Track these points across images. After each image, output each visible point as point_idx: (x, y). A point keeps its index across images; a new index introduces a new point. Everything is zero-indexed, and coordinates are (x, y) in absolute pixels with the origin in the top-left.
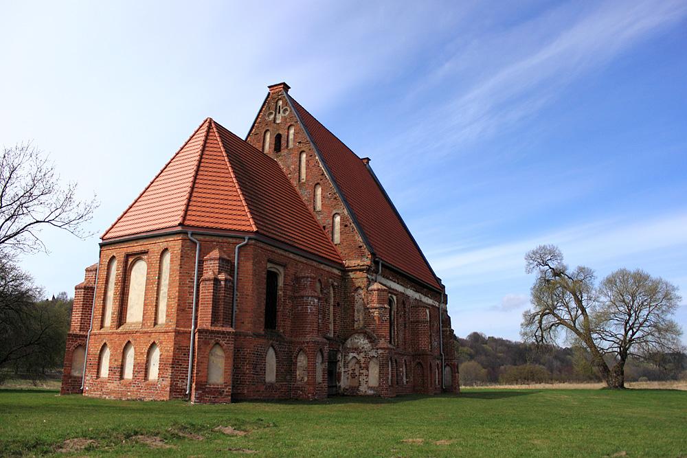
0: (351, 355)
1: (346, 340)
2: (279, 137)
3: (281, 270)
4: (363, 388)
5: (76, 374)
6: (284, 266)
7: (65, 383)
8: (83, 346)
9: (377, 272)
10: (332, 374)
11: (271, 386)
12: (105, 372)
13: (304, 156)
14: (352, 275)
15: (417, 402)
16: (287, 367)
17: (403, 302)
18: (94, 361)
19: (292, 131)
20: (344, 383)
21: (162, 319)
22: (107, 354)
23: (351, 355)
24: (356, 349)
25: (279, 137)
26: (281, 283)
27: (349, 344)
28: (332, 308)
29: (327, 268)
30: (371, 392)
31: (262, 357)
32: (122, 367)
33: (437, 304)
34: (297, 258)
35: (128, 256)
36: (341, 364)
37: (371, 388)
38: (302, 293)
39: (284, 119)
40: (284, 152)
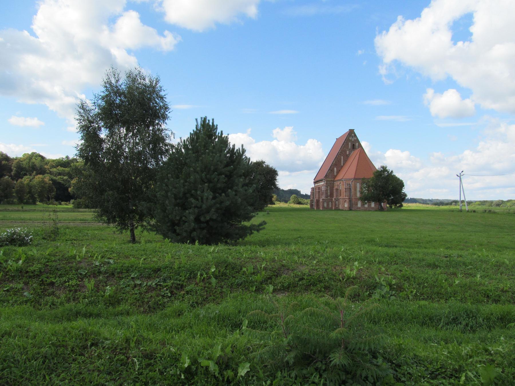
25: (354, 145)
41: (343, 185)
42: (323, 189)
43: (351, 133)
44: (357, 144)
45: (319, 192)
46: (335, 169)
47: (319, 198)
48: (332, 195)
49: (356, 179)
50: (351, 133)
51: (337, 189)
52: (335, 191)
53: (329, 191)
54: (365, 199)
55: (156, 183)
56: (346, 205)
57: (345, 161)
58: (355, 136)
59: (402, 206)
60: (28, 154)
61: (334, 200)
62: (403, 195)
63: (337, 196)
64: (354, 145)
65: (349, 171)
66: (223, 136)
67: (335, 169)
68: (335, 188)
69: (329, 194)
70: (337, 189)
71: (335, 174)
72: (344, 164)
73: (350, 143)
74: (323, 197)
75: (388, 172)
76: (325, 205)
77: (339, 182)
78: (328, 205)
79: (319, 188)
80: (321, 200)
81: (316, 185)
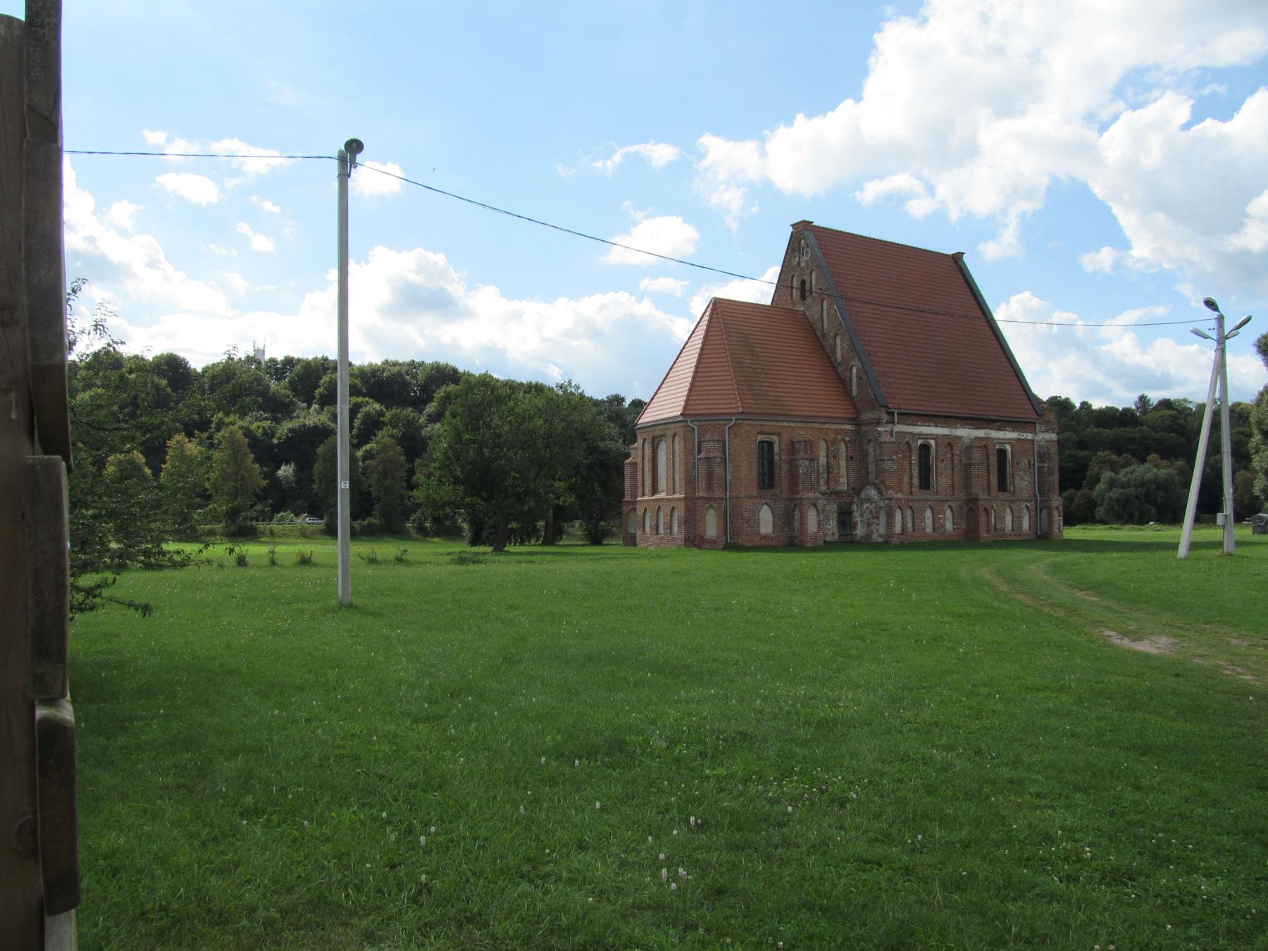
0: (866, 505)
1: (860, 491)
2: (803, 282)
3: (775, 438)
4: (875, 536)
5: (631, 531)
6: (779, 435)
7: (625, 539)
8: (634, 509)
9: (893, 422)
10: (845, 520)
11: (766, 537)
12: (648, 529)
13: (825, 303)
14: (865, 428)
15: (846, 553)
16: (787, 519)
17: (949, 444)
18: (639, 519)
19: (814, 276)
20: (860, 531)
21: (678, 489)
22: (648, 515)
23: (866, 505)
24: (869, 500)
25: (803, 282)
26: (776, 449)
27: (863, 495)
28: (843, 463)
29: (834, 426)
30: (880, 540)
31: (755, 514)
32: (657, 525)
33: (1030, 436)
34: (793, 425)
35: (654, 438)
36: (856, 514)
37: (881, 536)
38: (798, 456)
39: (807, 262)
40: (809, 300)
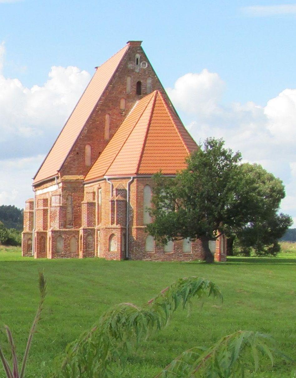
25: (139, 84)
41: (106, 192)
42: (56, 202)
43: (135, 51)
44: (149, 81)
45: (45, 212)
46: (88, 149)
47: (45, 227)
48: (76, 220)
49: (141, 177)
50: (135, 51)
51: (91, 205)
52: (84, 208)
53: (69, 209)
54: (165, 230)
55: (109, 107)
56: (115, 247)
57: (115, 127)
58: (144, 57)
59: (277, 249)
60: (273, 176)
61: (81, 232)
62: (281, 221)
63: (90, 222)
64: (139, 84)
65: (123, 155)
66: (78, 360)
67: (88, 149)
68: (85, 201)
69: (69, 216)
70: (91, 205)
71: (88, 162)
72: (111, 136)
73: (129, 80)
74: (55, 225)
75: (227, 158)
76: (60, 246)
77: (96, 186)
78: (67, 246)
79: (45, 201)
80: (49, 234)
81: (40, 192)
